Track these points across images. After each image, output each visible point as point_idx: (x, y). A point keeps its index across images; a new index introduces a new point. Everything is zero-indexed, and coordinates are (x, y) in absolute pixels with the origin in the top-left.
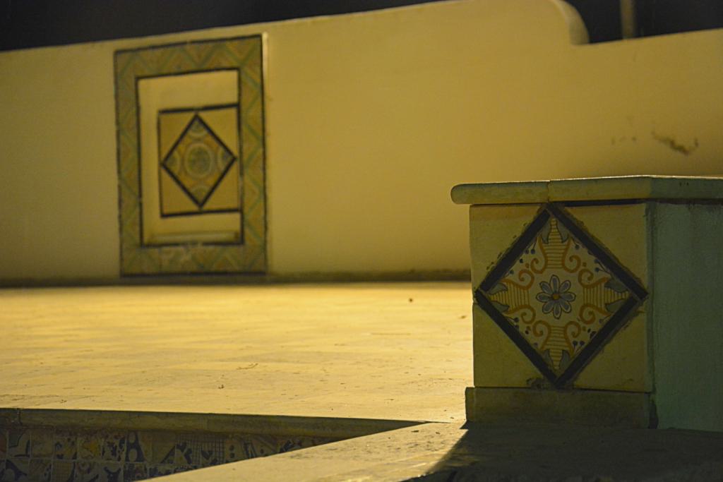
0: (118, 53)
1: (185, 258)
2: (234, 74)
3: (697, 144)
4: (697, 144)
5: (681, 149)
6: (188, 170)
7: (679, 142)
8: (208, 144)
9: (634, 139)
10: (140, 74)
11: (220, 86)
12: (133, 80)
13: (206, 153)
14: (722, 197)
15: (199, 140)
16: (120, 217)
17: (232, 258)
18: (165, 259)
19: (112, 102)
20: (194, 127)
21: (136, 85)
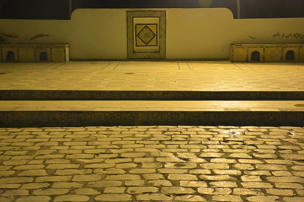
0: (127, 12)
1: (145, 55)
2: (159, 18)
3: (256, 38)
4: (256, 38)
5: (253, 38)
6: (144, 37)
7: (253, 37)
8: (149, 32)
9: (245, 36)
10: (134, 16)
11: (154, 20)
12: (132, 18)
13: (148, 34)
14: (2, 130)
15: (146, 31)
16: (127, 46)
17: (157, 55)
18: (140, 55)
19: (126, 22)
20: (145, 28)
21: (133, 19)
